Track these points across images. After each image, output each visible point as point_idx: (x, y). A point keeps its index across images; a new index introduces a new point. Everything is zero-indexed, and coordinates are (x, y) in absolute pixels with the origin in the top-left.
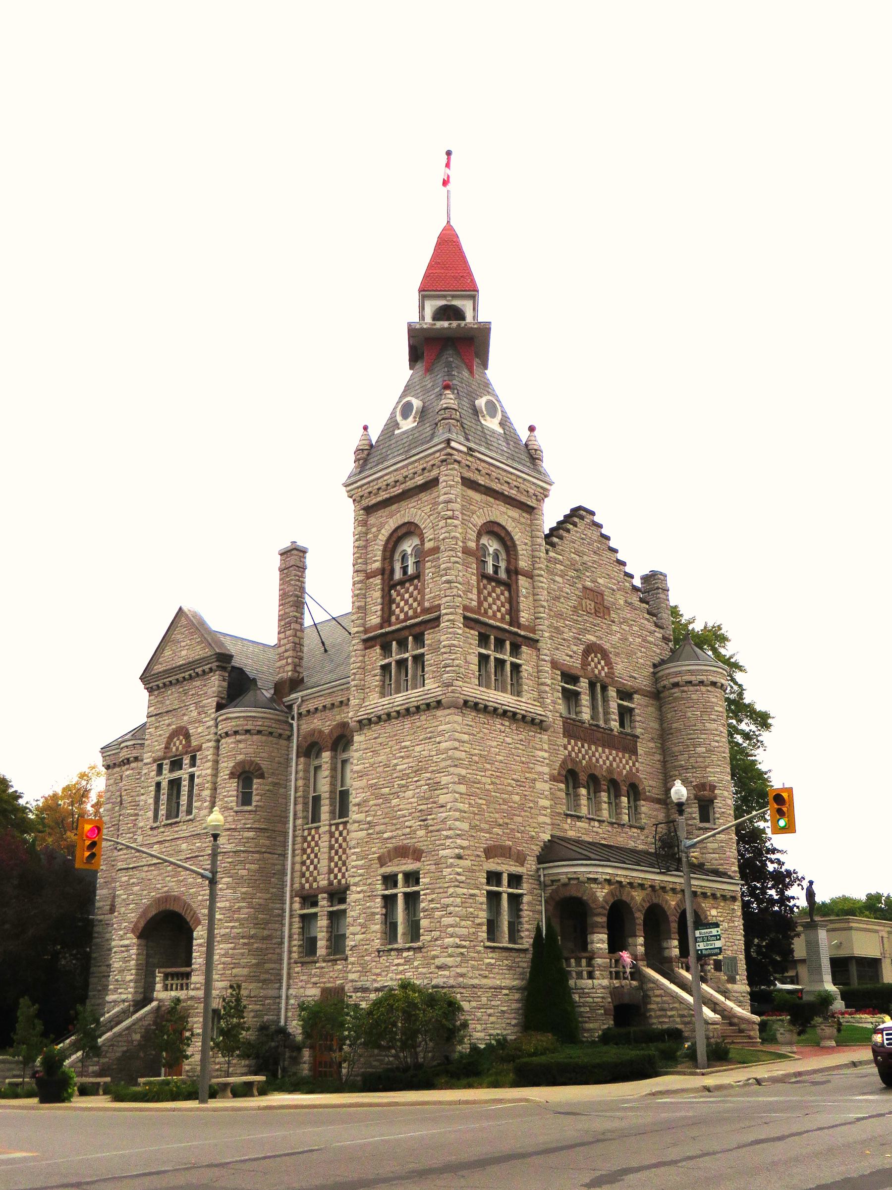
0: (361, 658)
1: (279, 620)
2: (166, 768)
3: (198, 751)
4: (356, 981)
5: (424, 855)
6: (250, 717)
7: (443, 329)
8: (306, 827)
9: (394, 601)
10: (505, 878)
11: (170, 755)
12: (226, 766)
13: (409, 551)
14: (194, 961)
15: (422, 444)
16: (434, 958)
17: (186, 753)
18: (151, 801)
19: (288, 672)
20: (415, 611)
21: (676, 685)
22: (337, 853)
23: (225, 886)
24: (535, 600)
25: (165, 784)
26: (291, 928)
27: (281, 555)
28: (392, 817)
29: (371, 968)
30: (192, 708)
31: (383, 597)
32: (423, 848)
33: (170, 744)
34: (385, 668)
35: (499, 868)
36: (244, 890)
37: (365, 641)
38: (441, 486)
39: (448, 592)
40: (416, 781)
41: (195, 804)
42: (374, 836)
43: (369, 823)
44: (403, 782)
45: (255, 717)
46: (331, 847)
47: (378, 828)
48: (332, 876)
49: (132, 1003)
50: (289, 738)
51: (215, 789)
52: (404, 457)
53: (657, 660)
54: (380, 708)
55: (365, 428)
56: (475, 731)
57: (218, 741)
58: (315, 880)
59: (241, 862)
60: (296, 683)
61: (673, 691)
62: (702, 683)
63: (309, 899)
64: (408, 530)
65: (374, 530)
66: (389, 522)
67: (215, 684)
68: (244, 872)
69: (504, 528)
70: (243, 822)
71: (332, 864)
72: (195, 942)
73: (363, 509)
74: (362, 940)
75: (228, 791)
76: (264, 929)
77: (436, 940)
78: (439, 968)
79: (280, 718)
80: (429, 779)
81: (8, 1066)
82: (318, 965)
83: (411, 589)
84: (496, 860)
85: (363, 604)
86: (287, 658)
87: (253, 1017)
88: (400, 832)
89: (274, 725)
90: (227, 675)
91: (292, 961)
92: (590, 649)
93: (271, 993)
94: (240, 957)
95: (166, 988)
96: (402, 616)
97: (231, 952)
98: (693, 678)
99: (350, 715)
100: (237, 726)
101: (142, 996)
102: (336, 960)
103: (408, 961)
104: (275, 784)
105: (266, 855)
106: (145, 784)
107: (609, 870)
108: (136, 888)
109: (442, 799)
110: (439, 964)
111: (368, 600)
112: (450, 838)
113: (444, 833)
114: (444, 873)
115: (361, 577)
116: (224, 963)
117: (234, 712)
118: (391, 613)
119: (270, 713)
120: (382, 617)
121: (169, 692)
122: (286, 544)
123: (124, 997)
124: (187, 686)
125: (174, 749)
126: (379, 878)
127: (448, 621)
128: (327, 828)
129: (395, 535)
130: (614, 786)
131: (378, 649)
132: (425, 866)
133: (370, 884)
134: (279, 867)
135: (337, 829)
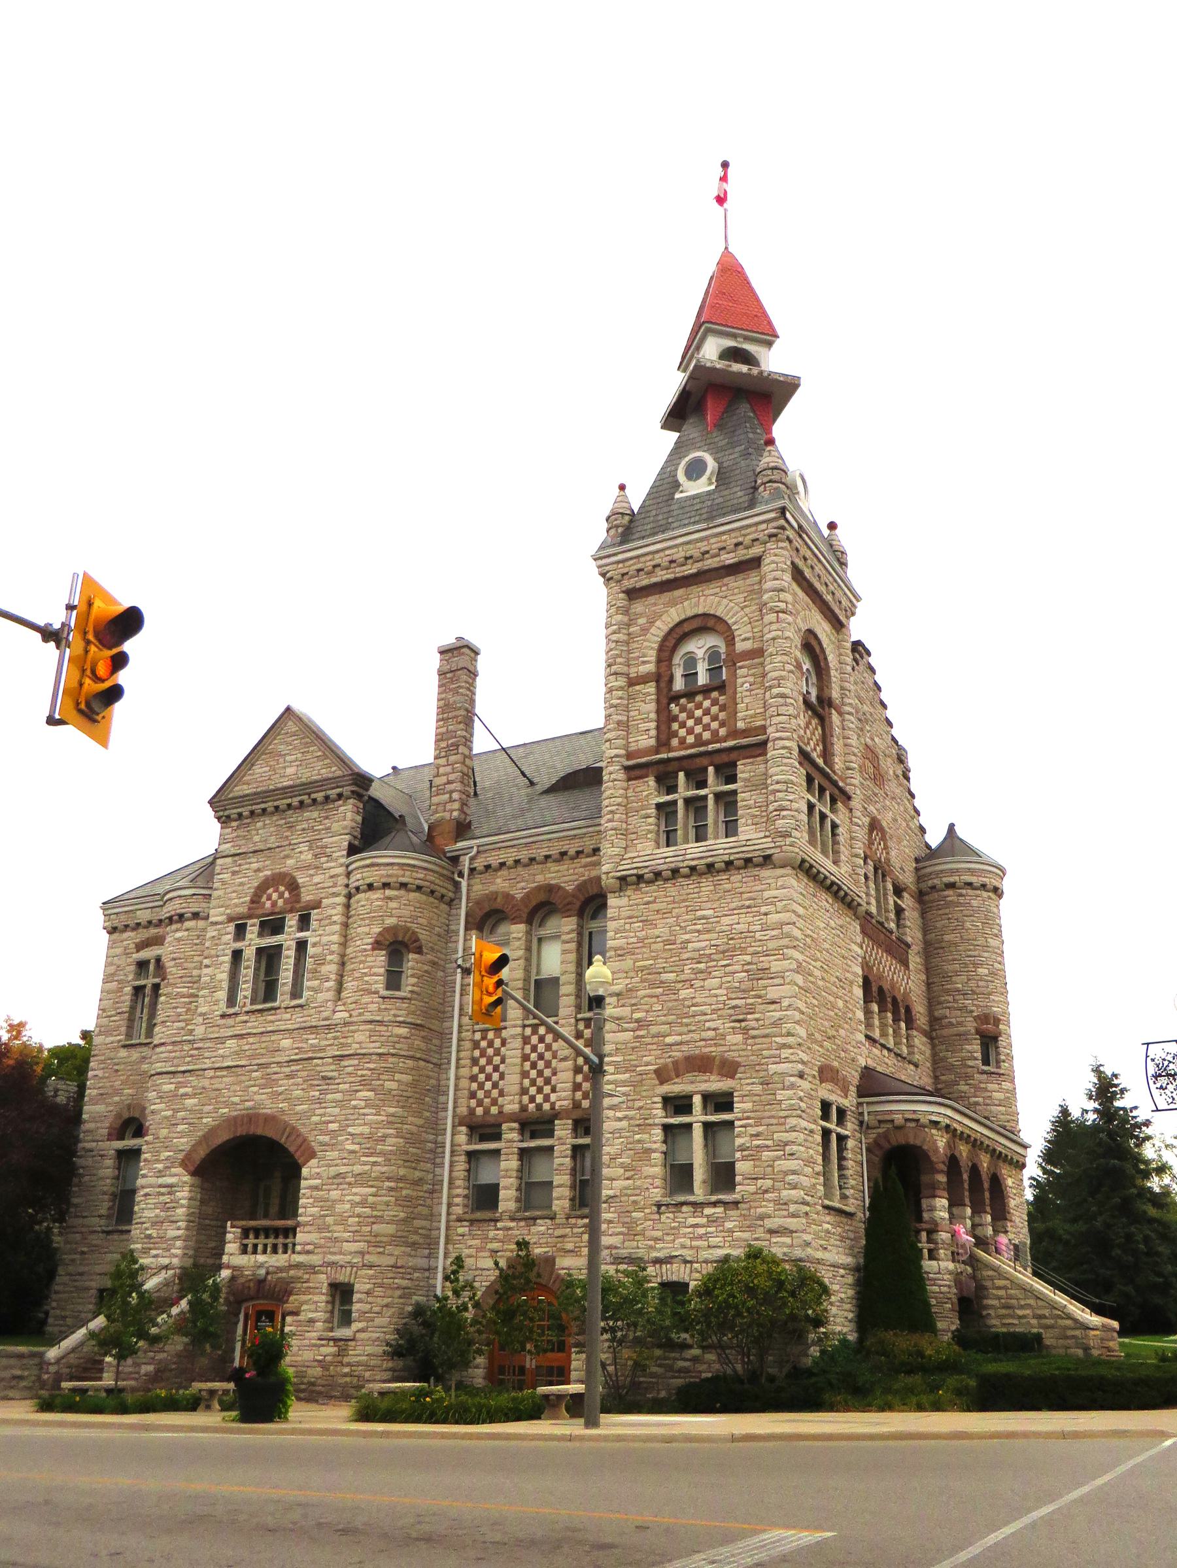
0: (621, 792)
1: (437, 741)
3: (314, 909)
4: (616, 1248)
5: (741, 1069)
7: (741, 374)
8: (477, 1027)
9: (675, 719)
10: (697, 1100)
11: (260, 912)
12: (365, 933)
13: (700, 653)
14: (301, 1211)
15: (735, 511)
16: (762, 1218)
17: (291, 911)
18: (224, 976)
19: (452, 811)
20: (715, 733)
21: (952, 886)
22: (534, 1065)
23: (363, 1103)
24: (846, 745)
25: (249, 954)
26: (451, 1172)
27: (441, 653)
28: (681, 1014)
29: (644, 1230)
30: (304, 847)
31: (658, 712)
32: (739, 1059)
33: (260, 897)
36: (392, 1110)
37: (627, 769)
39: (782, 710)
40: (725, 966)
41: (306, 984)
42: (648, 1040)
43: (638, 1021)
44: (702, 966)
45: (414, 866)
46: (525, 1058)
47: (654, 1029)
48: (526, 1099)
50: (452, 903)
51: (343, 964)
52: (704, 525)
54: (662, 861)
55: (622, 487)
56: (807, 903)
57: (349, 896)
58: (494, 1102)
59: (387, 1070)
60: (462, 829)
61: (946, 893)
62: (984, 886)
64: (705, 624)
65: (642, 621)
66: (672, 612)
67: (347, 815)
68: (393, 1085)
70: (392, 1012)
71: (526, 1082)
72: (303, 1183)
74: (626, 1188)
75: (371, 968)
76: (415, 1169)
77: (766, 1191)
78: (772, 1232)
79: (445, 872)
80: (749, 964)
82: (499, 1225)
85: (625, 718)
86: (451, 792)
87: (400, 1297)
88: (696, 1036)
89: (437, 881)
90: (361, 806)
91: (453, 1217)
93: (422, 1262)
94: (383, 1207)
95: (244, 1250)
96: (691, 739)
97: (371, 1199)
98: (973, 879)
99: (605, 868)
100: (388, 876)
101: (191, 1261)
102: (535, 1219)
103: (712, 1221)
104: (434, 963)
105: (422, 1063)
106: (213, 952)
107: (949, 1112)
108: (190, 1102)
109: (773, 993)
110: (774, 1227)
111: (632, 714)
112: (790, 1047)
113: (778, 1039)
114: (779, 1097)
115: (622, 682)
116: (359, 1216)
119: (435, 864)
120: (658, 738)
121: (259, 824)
122: (449, 640)
123: (166, 1261)
124: (292, 816)
126: (659, 1099)
127: (784, 748)
128: (519, 1030)
129: (680, 631)
131: (651, 781)
132: (743, 1087)
133: (640, 1108)
134: (433, 1082)
135: (535, 1032)
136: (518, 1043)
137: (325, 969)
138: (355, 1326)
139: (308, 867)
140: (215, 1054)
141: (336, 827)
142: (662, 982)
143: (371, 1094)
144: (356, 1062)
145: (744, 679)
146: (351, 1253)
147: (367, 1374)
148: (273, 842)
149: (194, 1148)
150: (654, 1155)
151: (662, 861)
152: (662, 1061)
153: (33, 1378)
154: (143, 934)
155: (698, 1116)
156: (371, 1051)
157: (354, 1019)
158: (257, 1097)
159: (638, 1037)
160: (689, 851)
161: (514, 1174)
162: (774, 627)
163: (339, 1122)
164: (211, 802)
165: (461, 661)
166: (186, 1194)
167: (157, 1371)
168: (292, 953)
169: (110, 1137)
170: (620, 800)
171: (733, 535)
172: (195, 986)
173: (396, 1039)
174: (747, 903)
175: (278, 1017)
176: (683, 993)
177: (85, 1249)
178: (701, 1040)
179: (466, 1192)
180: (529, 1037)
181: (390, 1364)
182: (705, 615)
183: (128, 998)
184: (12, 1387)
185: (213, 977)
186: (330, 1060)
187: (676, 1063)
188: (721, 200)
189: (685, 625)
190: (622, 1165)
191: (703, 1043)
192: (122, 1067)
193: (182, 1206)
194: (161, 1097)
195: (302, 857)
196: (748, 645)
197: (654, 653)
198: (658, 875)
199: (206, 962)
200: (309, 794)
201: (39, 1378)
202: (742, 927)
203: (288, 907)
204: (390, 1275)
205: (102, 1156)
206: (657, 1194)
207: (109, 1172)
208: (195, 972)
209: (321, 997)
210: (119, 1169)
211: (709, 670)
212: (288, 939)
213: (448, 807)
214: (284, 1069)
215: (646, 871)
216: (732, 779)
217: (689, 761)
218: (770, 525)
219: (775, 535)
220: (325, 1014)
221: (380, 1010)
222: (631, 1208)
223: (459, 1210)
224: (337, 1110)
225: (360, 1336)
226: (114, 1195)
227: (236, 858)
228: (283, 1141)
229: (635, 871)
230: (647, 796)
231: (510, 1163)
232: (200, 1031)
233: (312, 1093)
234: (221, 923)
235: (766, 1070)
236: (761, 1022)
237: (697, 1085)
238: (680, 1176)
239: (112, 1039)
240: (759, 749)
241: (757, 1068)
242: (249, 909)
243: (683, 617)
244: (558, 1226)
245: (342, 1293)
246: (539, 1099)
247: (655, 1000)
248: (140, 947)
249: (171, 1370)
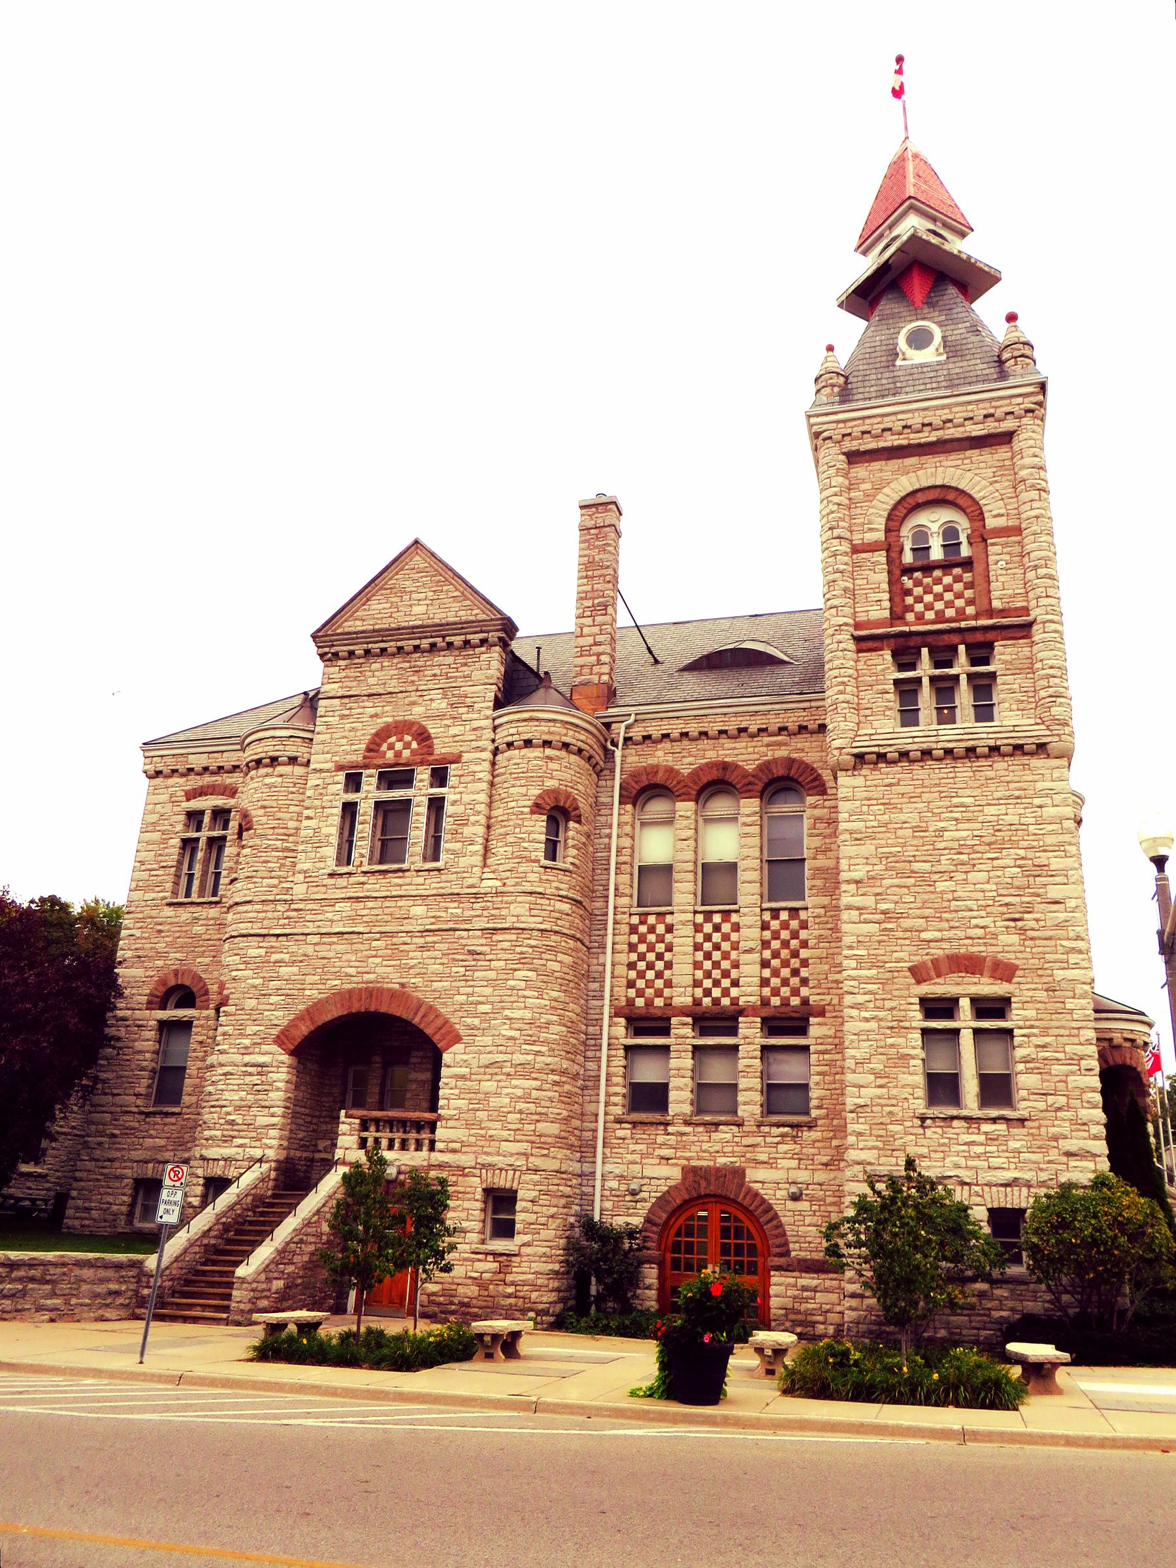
4: (869, 1164)
5: (1018, 973)
6: (572, 724)
10: (965, 1003)
11: (380, 762)
12: (520, 795)
13: (934, 527)
16: (1056, 1138)
17: (422, 763)
23: (523, 984)
25: (366, 809)
26: (610, 1066)
27: (582, 507)
28: (941, 911)
29: (905, 1145)
31: (890, 583)
32: (1017, 962)
33: (379, 745)
36: (555, 994)
42: (900, 934)
43: (883, 912)
44: (964, 857)
45: (577, 726)
46: (697, 947)
47: (906, 923)
48: (699, 992)
49: (273, 1165)
54: (910, 740)
55: (830, 348)
63: (648, 1023)
65: (866, 486)
66: (903, 479)
67: (491, 665)
68: (556, 966)
70: (555, 884)
73: (844, 454)
77: (1059, 1109)
78: (1069, 1154)
80: (1023, 858)
81: (102, 1273)
82: (670, 1129)
86: (599, 655)
87: (564, 1207)
94: (548, 1104)
96: (930, 615)
97: (535, 1094)
100: (550, 733)
102: (717, 1124)
103: (990, 1139)
106: (317, 803)
109: (1054, 892)
110: (1073, 1149)
111: (857, 582)
113: (1065, 943)
115: (845, 547)
116: (521, 1112)
117: (511, 714)
121: (376, 666)
122: (590, 496)
123: (258, 1153)
124: (420, 660)
128: (690, 916)
131: (887, 655)
136: (690, 930)
137: (467, 831)
138: (519, 1239)
139: (441, 717)
140: (320, 917)
141: (477, 675)
142: (913, 872)
143: (532, 974)
144: (514, 937)
145: (998, 555)
146: (512, 1155)
147: (534, 1295)
148: (393, 685)
149: (293, 1024)
150: (913, 1062)
151: (910, 740)
152: (918, 958)
153: (130, 1293)
154: (194, 782)
155: (965, 1019)
156: (533, 926)
157: (511, 889)
158: (379, 970)
159: (886, 930)
160: (941, 732)
161: (689, 1074)
162: (1035, 505)
163: (492, 1003)
164: (314, 637)
165: (602, 518)
166: (283, 1076)
167: (287, 1287)
168: (424, 810)
169: (150, 1005)
170: (851, 672)
171: (981, 406)
172: (291, 839)
173: (557, 915)
174: (1017, 793)
175: (407, 881)
176: (941, 886)
177: (117, 1132)
178: (967, 938)
179: (624, 1091)
180: (701, 925)
181: (556, 1284)
182: (943, 486)
183: (176, 851)
184: (107, 1305)
185: (316, 830)
186: (479, 933)
187: (935, 962)
188: (898, 93)
189: (919, 495)
190: (872, 1072)
191: (970, 941)
192: (167, 927)
193: (278, 1089)
194: (246, 963)
195: (434, 705)
196: (1001, 522)
197: (883, 521)
198: (904, 755)
199: (306, 813)
200: (444, 637)
201: (136, 1292)
202: (1010, 819)
203: (418, 758)
204: (556, 1181)
205: (139, 1026)
206: (919, 1105)
207: (150, 1045)
208: (291, 824)
209: (463, 862)
210: (160, 1042)
211: (944, 546)
212: (420, 791)
213: (596, 669)
214: (415, 940)
215: (890, 749)
217: (936, 637)
218: (1026, 400)
219: (1032, 411)
220: (470, 881)
221: (541, 880)
222: (886, 1120)
223: (618, 1110)
224: (488, 991)
225: (525, 1250)
226: (153, 1071)
227: (346, 700)
228: (416, 1021)
229: (876, 749)
230: (884, 670)
232: (299, 890)
233: (454, 970)
234: (328, 771)
235: (1051, 976)
236: (1042, 923)
238: (943, 1087)
239: (153, 895)
241: (1040, 972)
242: (365, 757)
243: (917, 486)
244: (747, 1134)
245: (500, 1203)
246: (716, 993)
247: (905, 890)
248: (190, 795)
249: (297, 1285)
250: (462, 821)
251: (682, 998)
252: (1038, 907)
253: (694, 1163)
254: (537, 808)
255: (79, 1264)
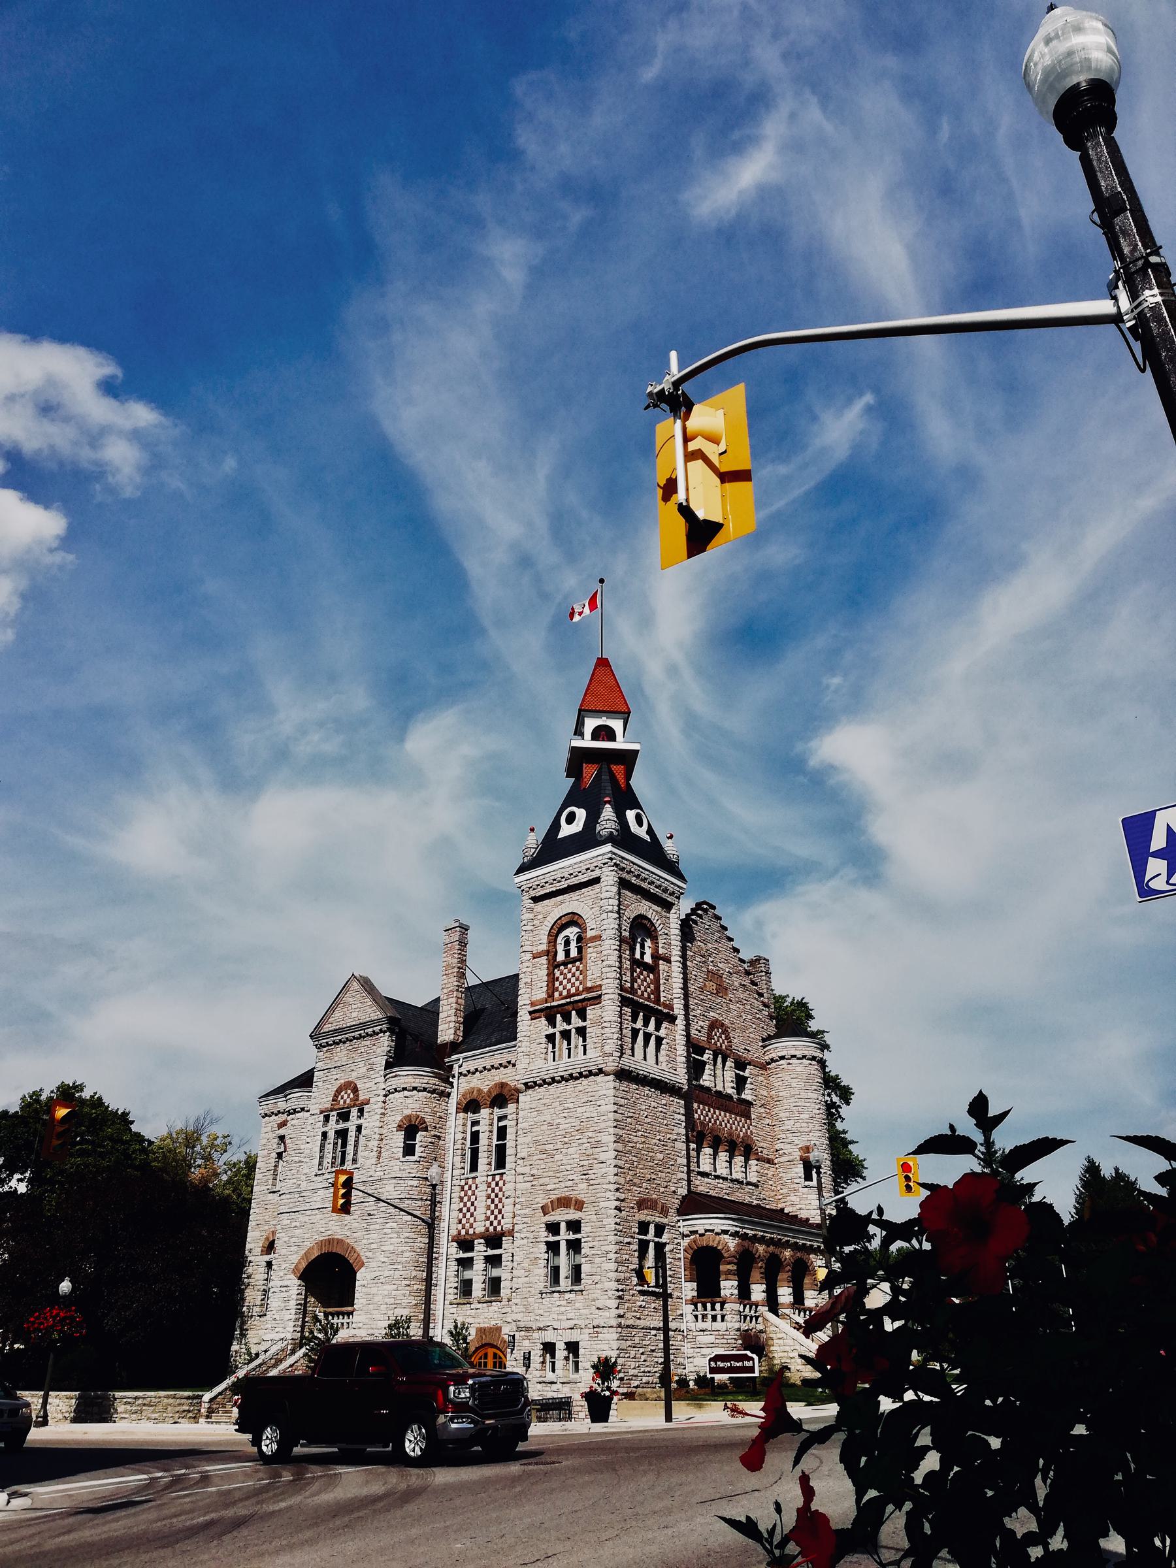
2: (333, 1119)
10: (563, 1226)
12: (395, 1119)
17: (354, 1106)
20: (577, 989)
25: (331, 1135)
30: (361, 1064)
31: (548, 975)
34: (551, 1038)
35: (649, 1218)
37: (531, 1013)
38: (602, 884)
44: (566, 1140)
46: (489, 1197)
47: (541, 1181)
48: (488, 1223)
53: (765, 1035)
64: (573, 920)
67: (385, 1043)
69: (649, 920)
82: (473, 1306)
83: (574, 969)
84: (645, 1212)
88: (563, 1185)
92: (714, 1025)
97: (394, 1293)
108: (298, 1232)
118: (555, 989)
125: (342, 1102)
129: (564, 920)
130: (266, 1115)
131: (543, 1020)
148: (344, 1061)
149: (299, 1262)
198: (553, 1080)
212: (351, 1125)
216: (584, 1020)
231: (479, 1265)
237: (563, 1216)
240: (597, 999)
250: (369, 1139)
251: (480, 1228)
252: (595, 1166)
253: (482, 1325)
254: (399, 1128)
255: (167, 1397)
